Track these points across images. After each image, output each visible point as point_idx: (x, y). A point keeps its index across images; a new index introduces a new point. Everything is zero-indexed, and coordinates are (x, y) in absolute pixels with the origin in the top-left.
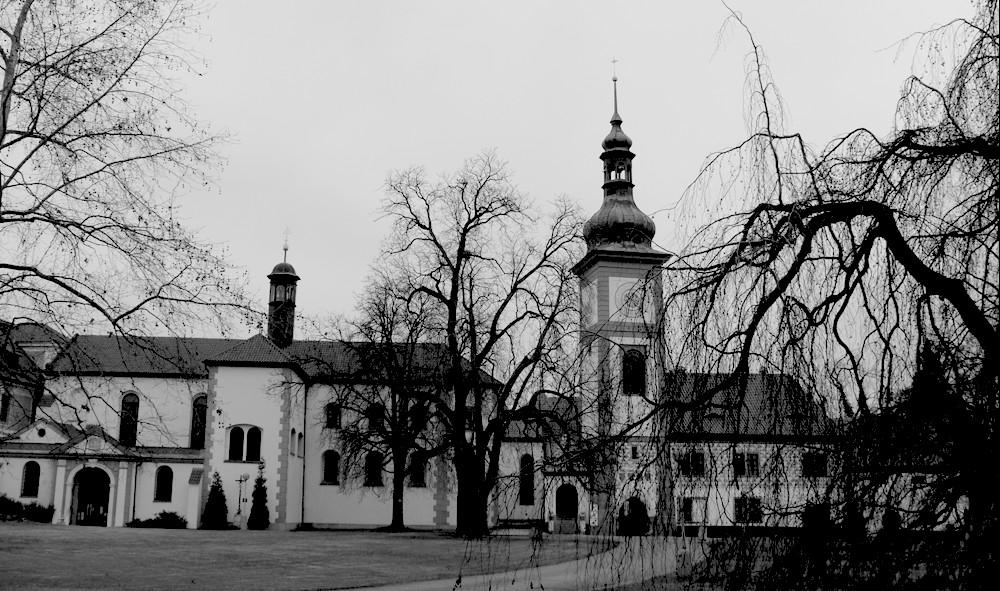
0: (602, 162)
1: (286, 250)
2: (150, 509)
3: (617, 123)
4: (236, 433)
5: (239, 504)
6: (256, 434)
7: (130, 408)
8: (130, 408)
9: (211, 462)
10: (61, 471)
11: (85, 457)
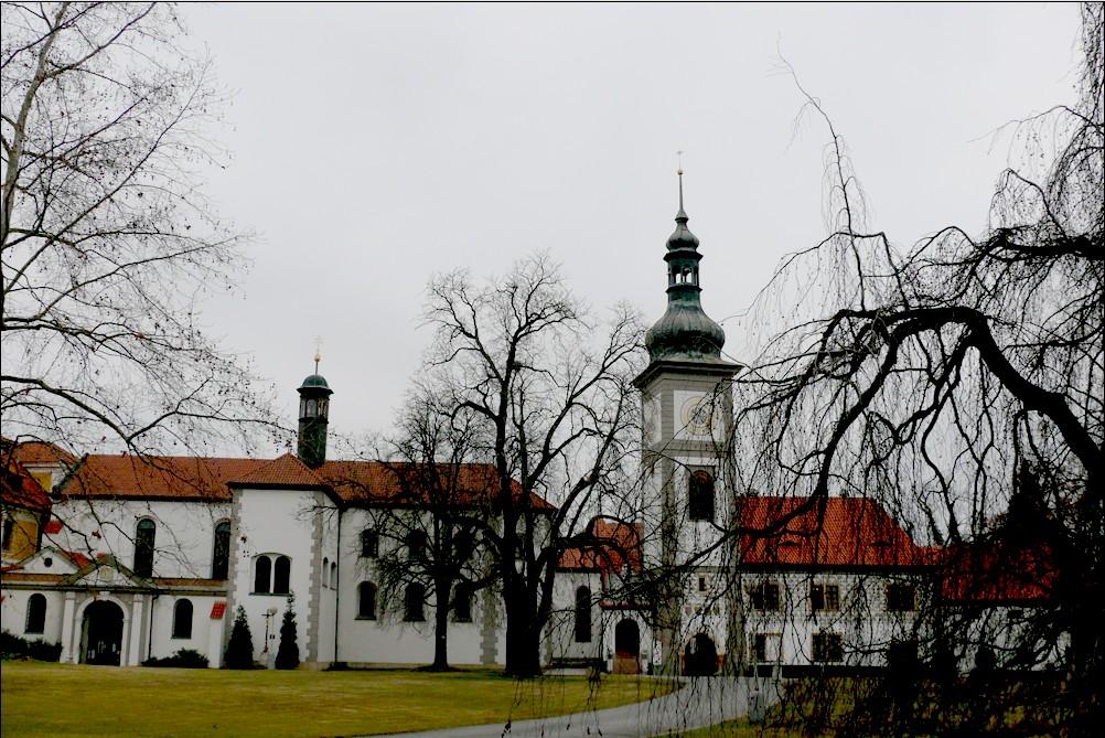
0: (666, 263)
1: (317, 360)
2: (167, 647)
3: (682, 220)
4: (262, 563)
5: (265, 641)
6: (284, 563)
7: (145, 534)
8: (145, 534)
9: (235, 594)
10: (70, 605)
11: (96, 589)
